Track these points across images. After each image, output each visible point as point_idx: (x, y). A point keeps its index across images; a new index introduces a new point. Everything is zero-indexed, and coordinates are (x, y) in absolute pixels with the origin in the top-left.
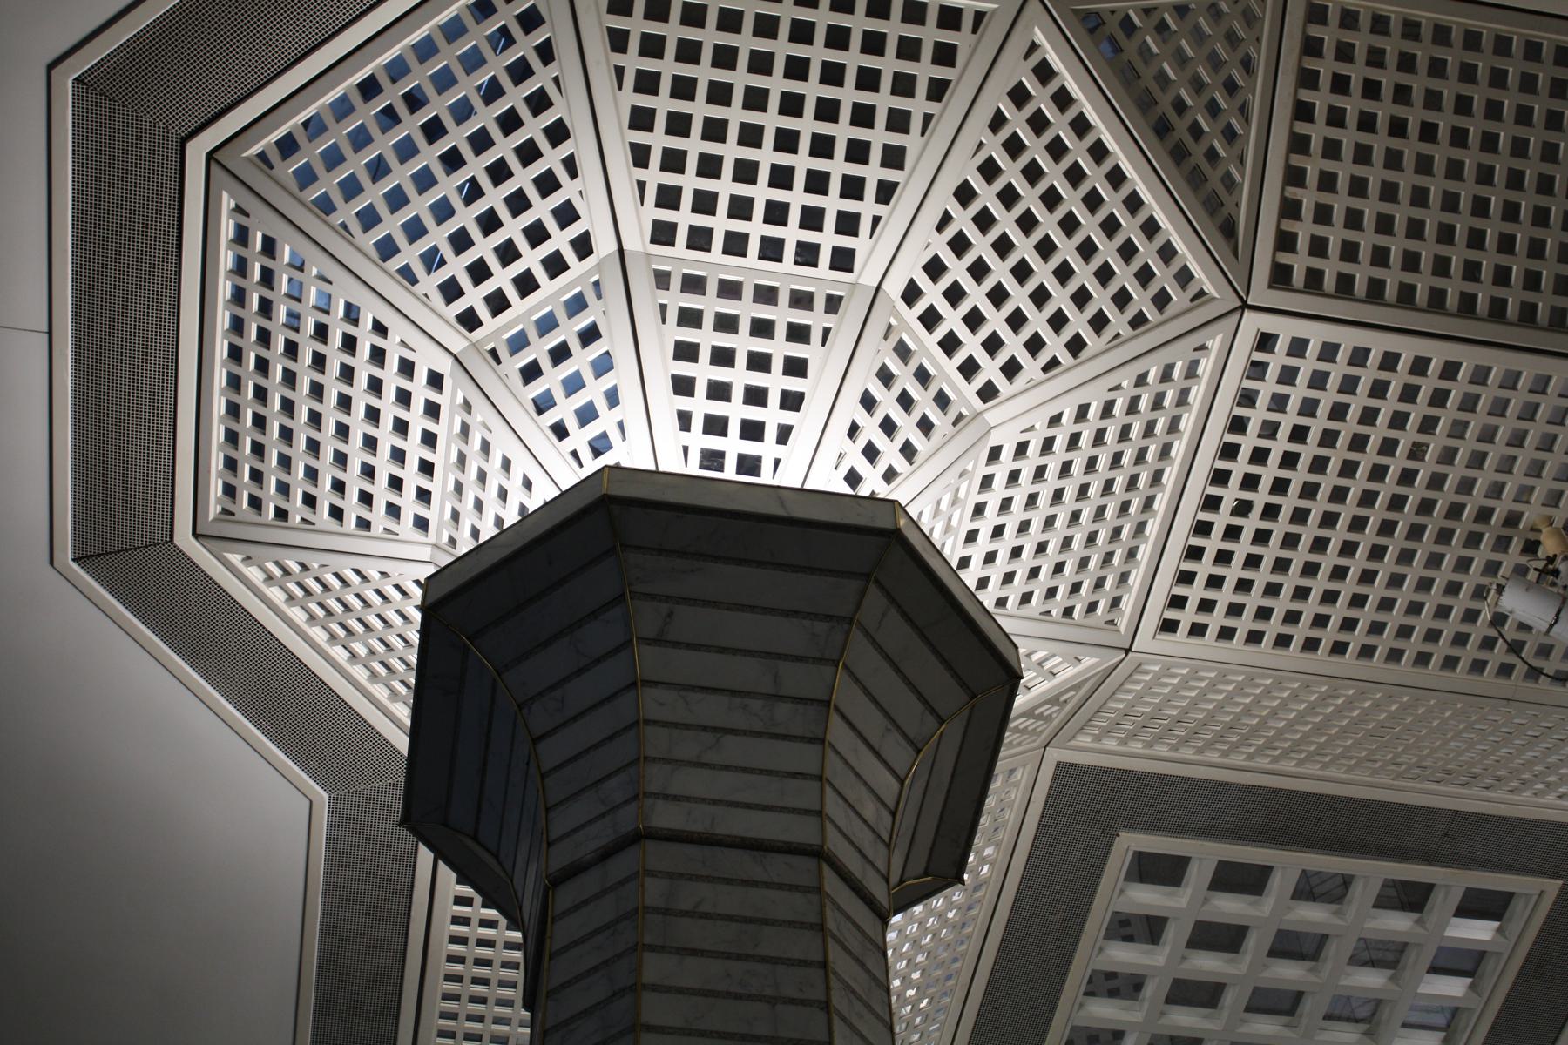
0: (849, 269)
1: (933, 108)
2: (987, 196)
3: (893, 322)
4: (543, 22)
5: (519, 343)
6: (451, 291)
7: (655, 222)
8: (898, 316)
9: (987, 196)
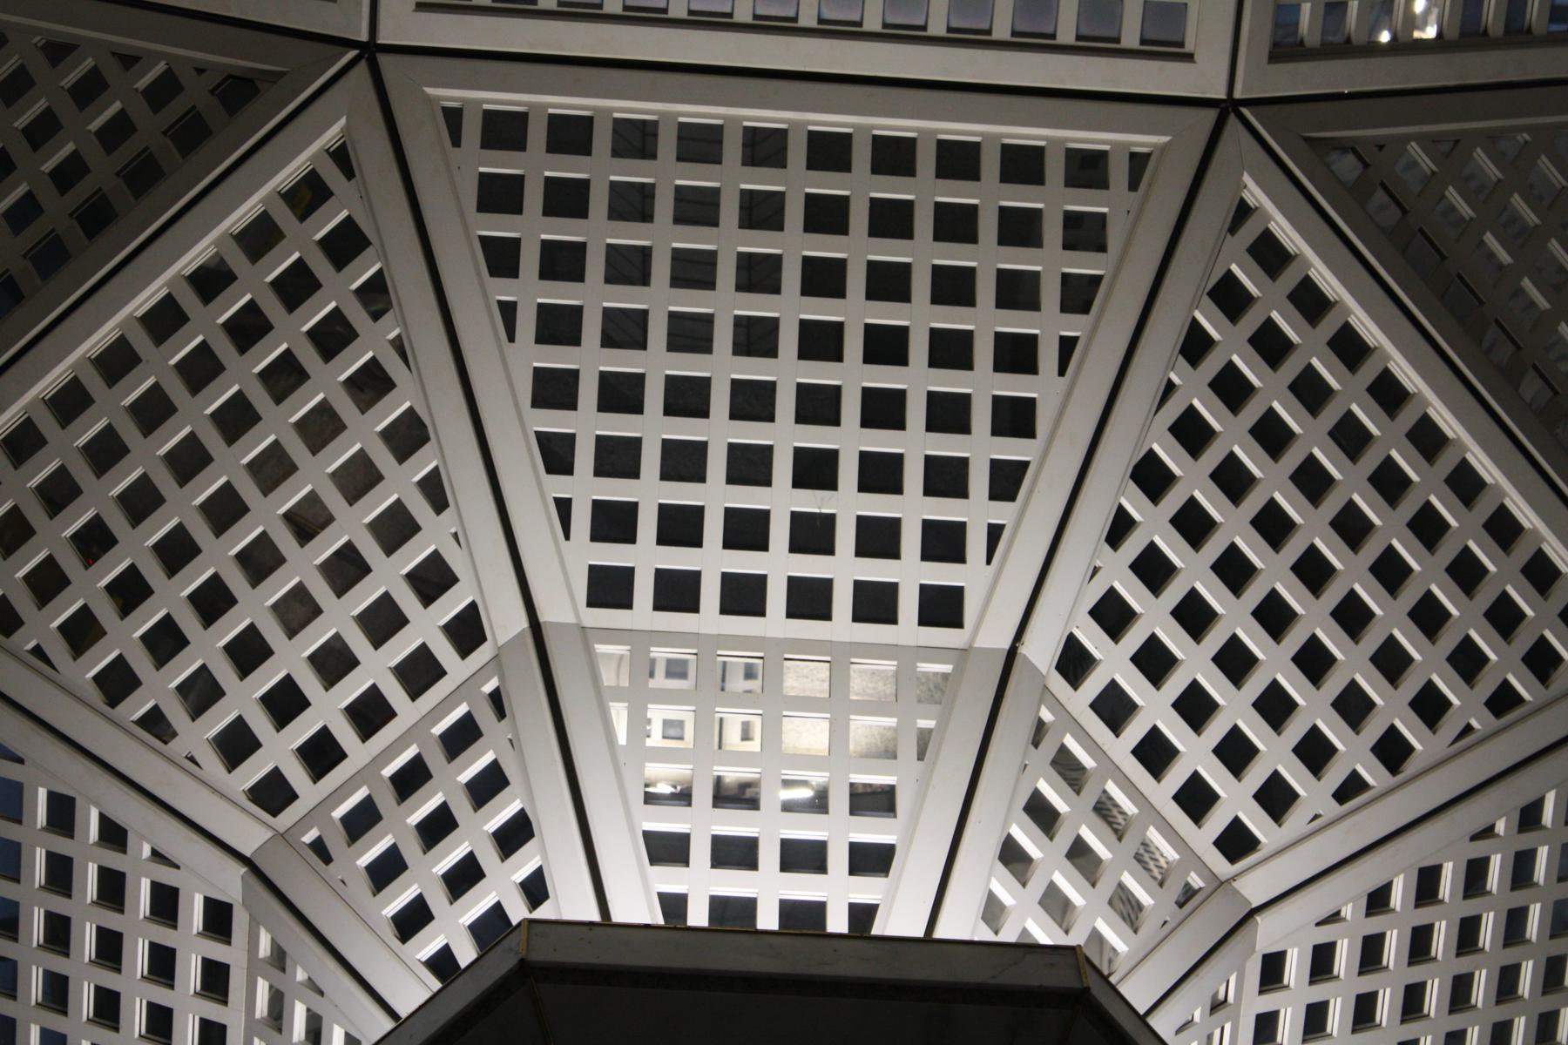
0: (956, 622)
1: (1002, 513)
2: (1193, 480)
3: (1046, 715)
4: (367, 243)
5: (362, 821)
6: (236, 745)
7: (593, 570)
8: (1058, 706)
9: (1193, 480)
